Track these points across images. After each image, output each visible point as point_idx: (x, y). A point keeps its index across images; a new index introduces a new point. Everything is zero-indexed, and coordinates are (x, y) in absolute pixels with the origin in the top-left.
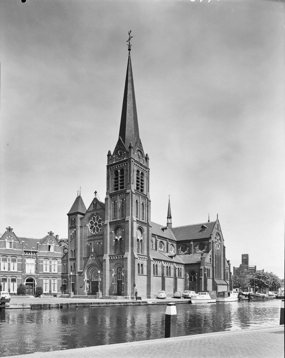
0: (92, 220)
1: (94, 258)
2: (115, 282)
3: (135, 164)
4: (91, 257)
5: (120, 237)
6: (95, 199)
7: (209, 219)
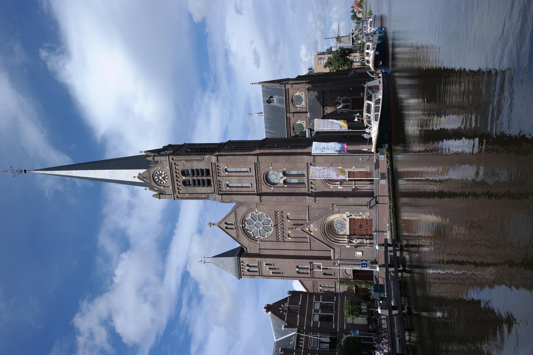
0: (251, 233)
2: (352, 184)
3: (177, 153)
7: (257, 83)
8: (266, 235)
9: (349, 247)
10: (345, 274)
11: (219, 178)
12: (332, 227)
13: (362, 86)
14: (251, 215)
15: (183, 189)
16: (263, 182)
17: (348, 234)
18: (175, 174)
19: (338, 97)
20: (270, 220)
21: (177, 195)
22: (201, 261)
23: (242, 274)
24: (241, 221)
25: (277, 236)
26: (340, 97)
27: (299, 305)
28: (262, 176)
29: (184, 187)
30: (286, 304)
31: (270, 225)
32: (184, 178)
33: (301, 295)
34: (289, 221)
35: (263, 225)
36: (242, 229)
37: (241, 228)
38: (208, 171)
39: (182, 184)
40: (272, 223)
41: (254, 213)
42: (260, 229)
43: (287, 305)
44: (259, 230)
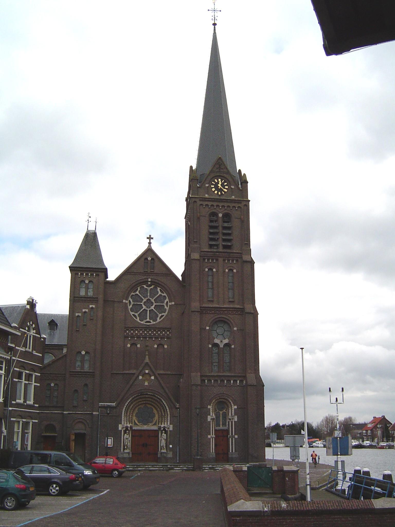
0: (137, 293)
1: (153, 378)
2: (212, 435)
4: (143, 376)
5: (226, 341)
6: (149, 251)
8: (133, 313)
9: (120, 429)
10: (77, 421)
11: (221, 260)
12: (144, 405)
13: (26, 405)
14: (163, 294)
15: (205, 212)
16: (216, 317)
17: (135, 428)
18: (226, 204)
19: (236, 407)
20: (156, 320)
21: (198, 203)
22: (90, 217)
23: (78, 272)
24: (156, 281)
25: (132, 329)
26: (235, 409)
27: (32, 351)
28: (224, 316)
29: (209, 213)
30: (35, 331)
31: (148, 320)
32: (220, 215)
33: (41, 355)
34: (156, 346)
35: (149, 310)
36: (144, 280)
37: (146, 280)
38: (229, 247)
39: (212, 211)
40: (153, 323)
41: (167, 300)
42: (144, 306)
43: (33, 332)
44: (142, 303)
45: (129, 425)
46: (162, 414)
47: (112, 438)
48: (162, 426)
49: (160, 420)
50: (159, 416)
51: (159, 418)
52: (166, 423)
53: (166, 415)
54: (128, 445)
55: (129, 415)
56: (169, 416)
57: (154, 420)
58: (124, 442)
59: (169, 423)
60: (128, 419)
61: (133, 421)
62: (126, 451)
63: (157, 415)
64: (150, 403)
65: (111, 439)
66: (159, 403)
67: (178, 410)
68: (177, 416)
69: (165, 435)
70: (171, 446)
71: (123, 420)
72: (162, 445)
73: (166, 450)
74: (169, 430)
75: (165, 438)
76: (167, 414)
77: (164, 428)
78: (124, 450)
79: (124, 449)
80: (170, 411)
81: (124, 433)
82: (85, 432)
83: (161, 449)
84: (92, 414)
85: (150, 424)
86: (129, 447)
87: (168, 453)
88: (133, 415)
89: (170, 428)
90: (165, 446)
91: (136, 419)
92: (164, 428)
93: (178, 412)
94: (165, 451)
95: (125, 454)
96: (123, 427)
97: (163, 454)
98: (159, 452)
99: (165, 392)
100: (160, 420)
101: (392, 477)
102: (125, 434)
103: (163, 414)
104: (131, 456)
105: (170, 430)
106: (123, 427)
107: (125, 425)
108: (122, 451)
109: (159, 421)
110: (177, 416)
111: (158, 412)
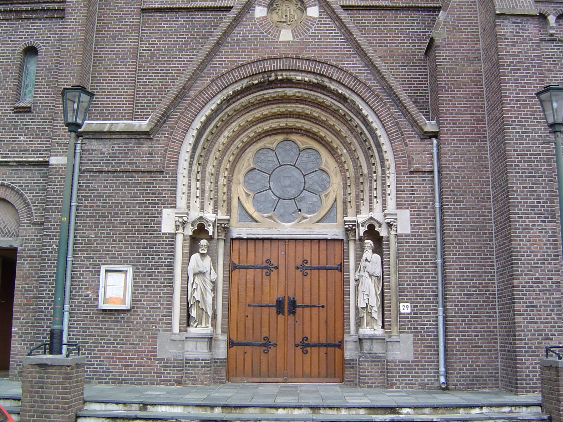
9: (167, 226)
12: (280, 138)
45: (210, 216)
46: (358, 167)
47: (130, 270)
48: (362, 218)
49: (352, 197)
50: (345, 178)
51: (345, 187)
52: (377, 207)
53: (379, 169)
54: (205, 302)
55: (216, 175)
56: (393, 170)
57: (324, 201)
58: (185, 291)
59: (391, 203)
60: (207, 188)
61: (235, 203)
62: (193, 330)
63: (339, 175)
64: (306, 125)
65: (126, 272)
66: (343, 119)
67: (432, 144)
68: (432, 172)
69: (377, 257)
70: (406, 308)
71: (181, 189)
72: (362, 304)
73: (383, 327)
74: (393, 233)
75: (378, 272)
76: (384, 172)
77: (371, 228)
78: (188, 325)
79: (188, 320)
80: (394, 151)
81: (187, 249)
82: (15, 245)
83: (359, 324)
84: (46, 164)
85: (309, 216)
86: (210, 313)
87: (395, 338)
88: (234, 180)
89: (399, 224)
90: (375, 309)
91: (248, 195)
92: (371, 228)
93: (435, 150)
94: (378, 331)
95: (190, 346)
96: (184, 223)
97: (366, 346)
98: (347, 337)
99: (371, 65)
100: (352, 197)
101: (19, 274)
102: (191, 254)
103: (365, 171)
104: (221, 351)
105: (399, 232)
106: (184, 223)
107: (195, 214)
108: (176, 328)
109: (345, 203)
110: (427, 169)
111: (341, 164)
